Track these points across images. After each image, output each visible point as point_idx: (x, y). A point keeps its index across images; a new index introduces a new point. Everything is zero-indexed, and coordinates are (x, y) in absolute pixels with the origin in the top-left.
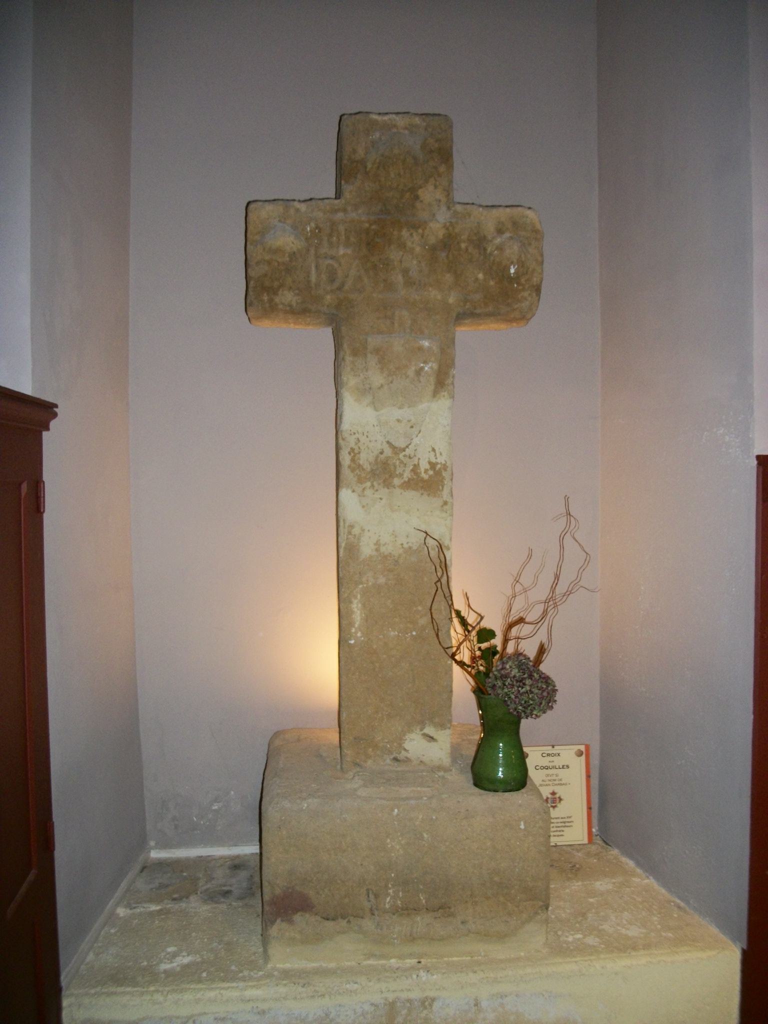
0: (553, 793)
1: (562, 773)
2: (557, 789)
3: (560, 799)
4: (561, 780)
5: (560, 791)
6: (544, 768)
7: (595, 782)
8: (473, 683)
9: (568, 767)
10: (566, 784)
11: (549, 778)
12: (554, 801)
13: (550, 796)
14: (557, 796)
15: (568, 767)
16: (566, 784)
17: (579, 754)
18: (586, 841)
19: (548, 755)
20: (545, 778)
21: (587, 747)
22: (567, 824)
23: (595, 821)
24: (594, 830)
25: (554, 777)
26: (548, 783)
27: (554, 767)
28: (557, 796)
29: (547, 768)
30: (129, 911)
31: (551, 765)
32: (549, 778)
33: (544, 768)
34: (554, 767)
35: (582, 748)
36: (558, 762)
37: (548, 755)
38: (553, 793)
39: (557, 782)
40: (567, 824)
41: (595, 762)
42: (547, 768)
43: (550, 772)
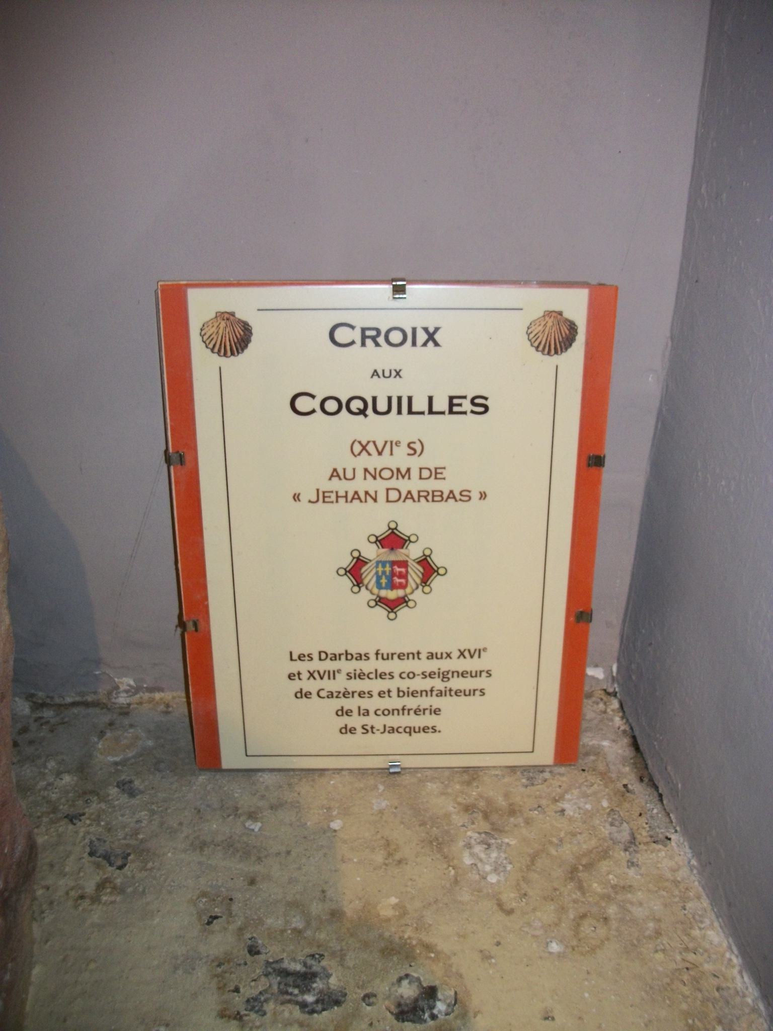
0: (393, 540)
1: (443, 437)
2: (408, 518)
3: (429, 570)
4: (436, 473)
5: (427, 528)
6: (344, 406)
7: (625, 479)
8: (421, 569)
9: (481, 405)
10: (465, 496)
11: (374, 462)
12: (396, 575)
13: (371, 552)
14: (414, 552)
15: (481, 405)
16: (465, 496)
17: (555, 337)
18: (546, 753)
19: (371, 336)
20: (348, 462)
21: (603, 305)
22: (456, 683)
23: (605, 634)
24: (595, 672)
25: (400, 459)
26: (361, 485)
27: (403, 406)
28: (414, 552)
29: (366, 407)
30: (571, 910)
31: (382, 390)
32: (374, 462)
33: (344, 406)
34: (403, 406)
35: (575, 305)
36: (421, 374)
37: (371, 336)
38: (393, 540)
39: (414, 485)
40: (456, 683)
41: (640, 378)
42: (366, 407)
43: (372, 428)
